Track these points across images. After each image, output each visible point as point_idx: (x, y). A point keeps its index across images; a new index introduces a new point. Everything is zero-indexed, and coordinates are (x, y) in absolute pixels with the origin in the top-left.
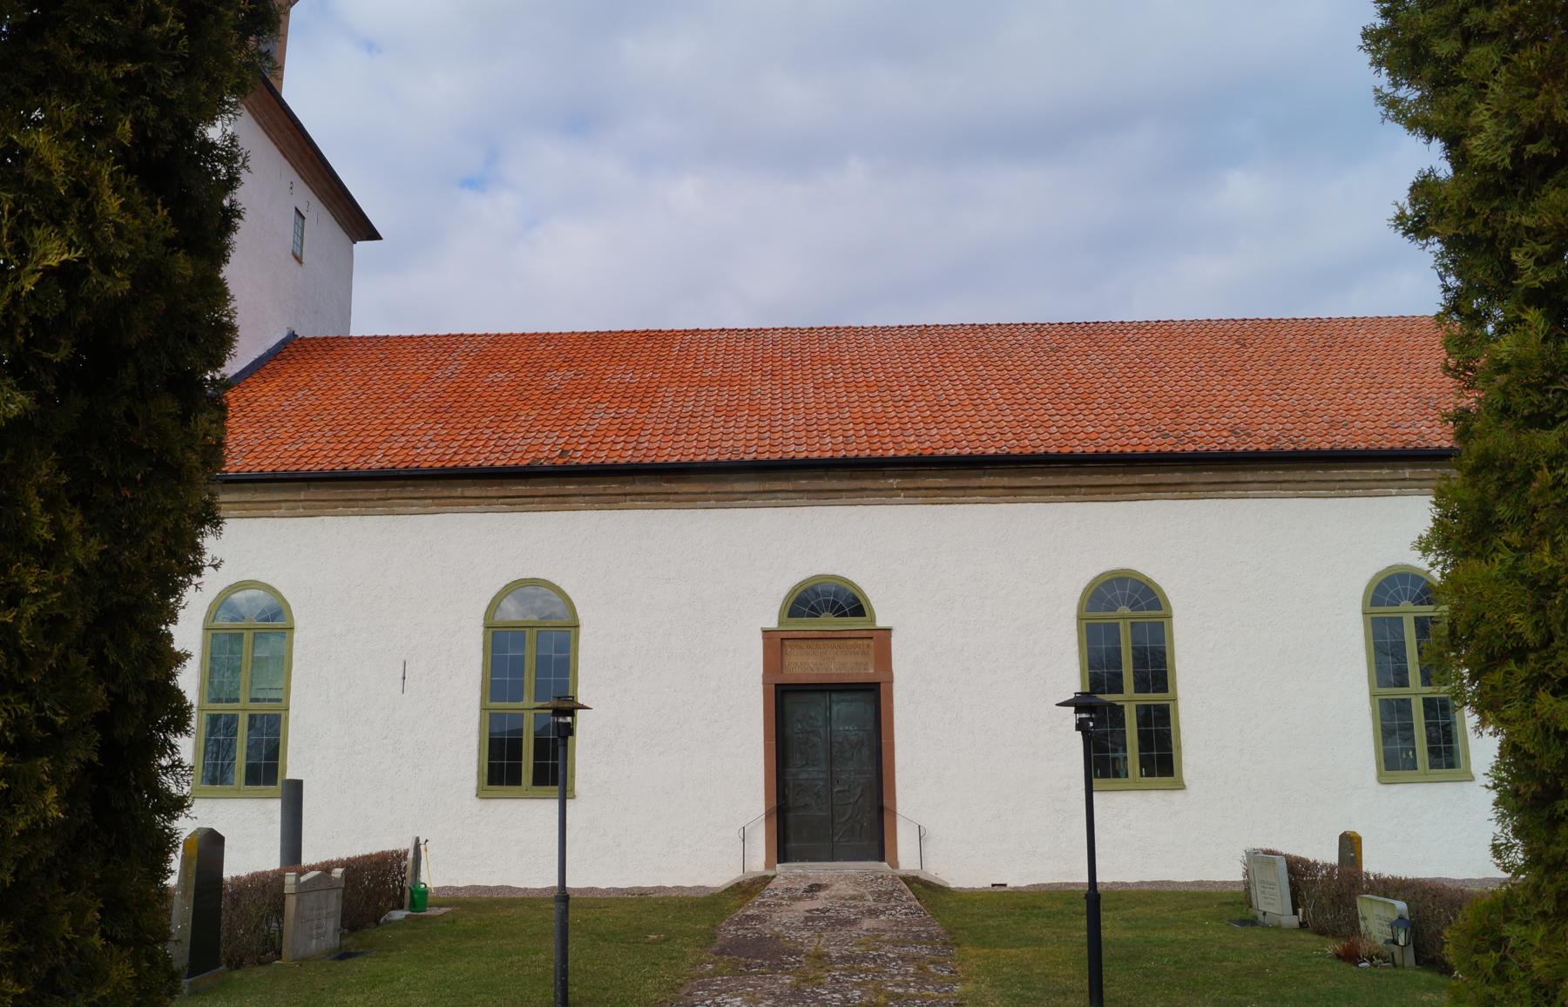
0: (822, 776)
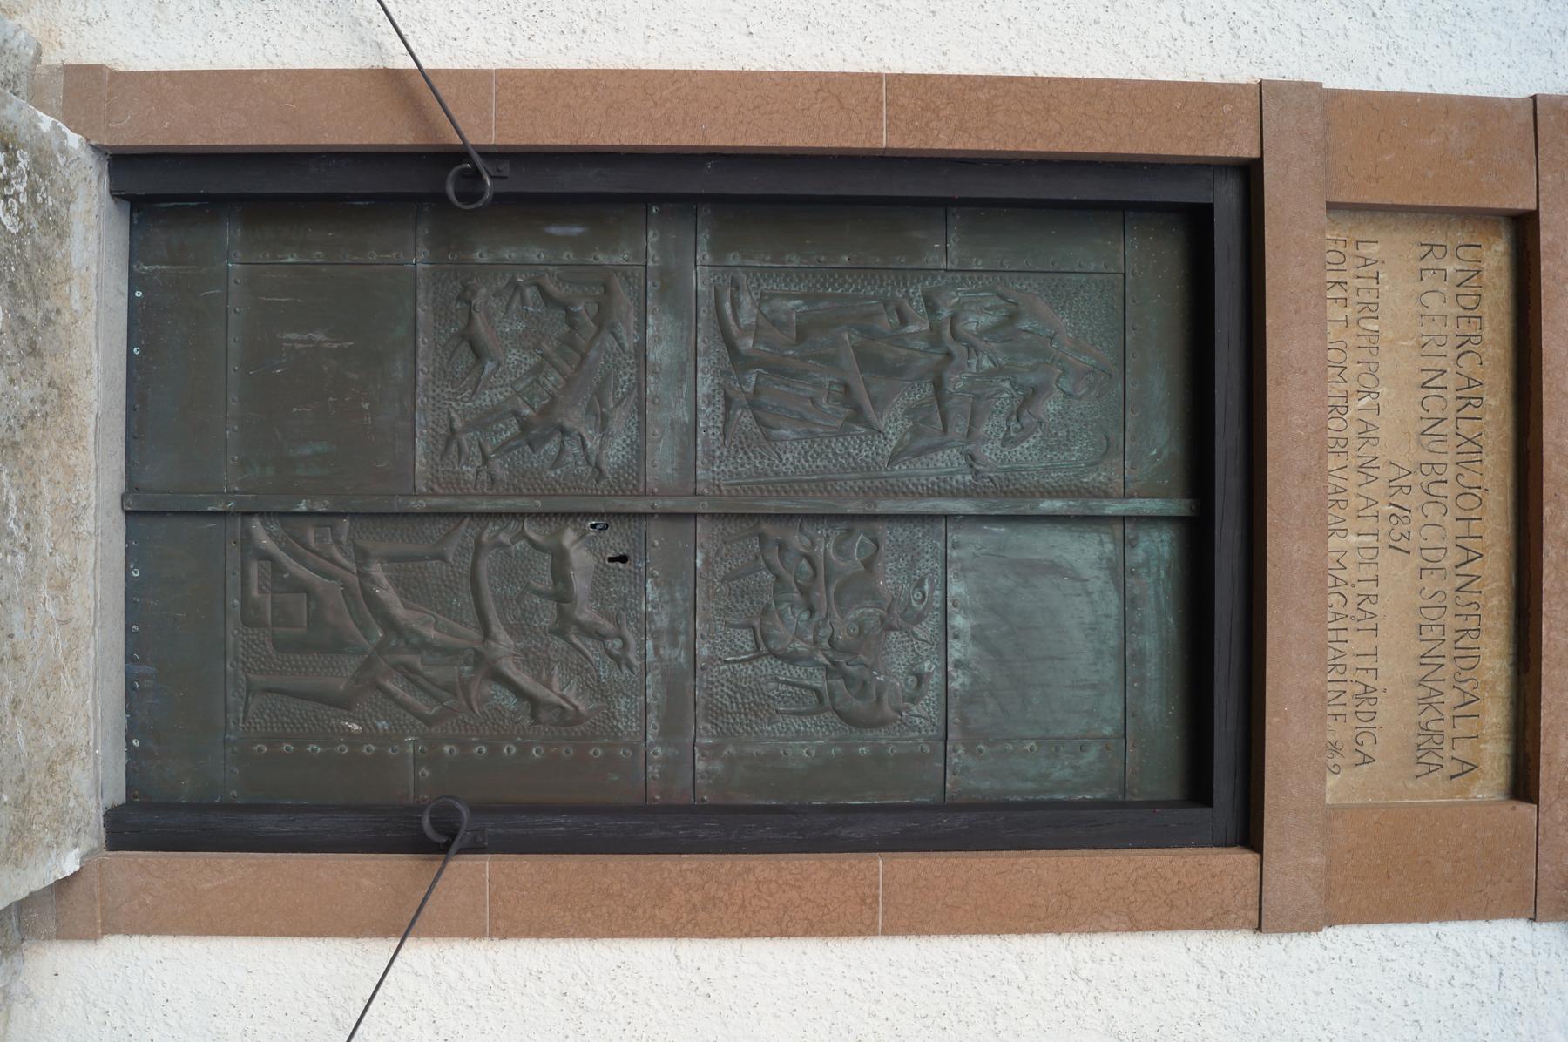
0: (662, 460)
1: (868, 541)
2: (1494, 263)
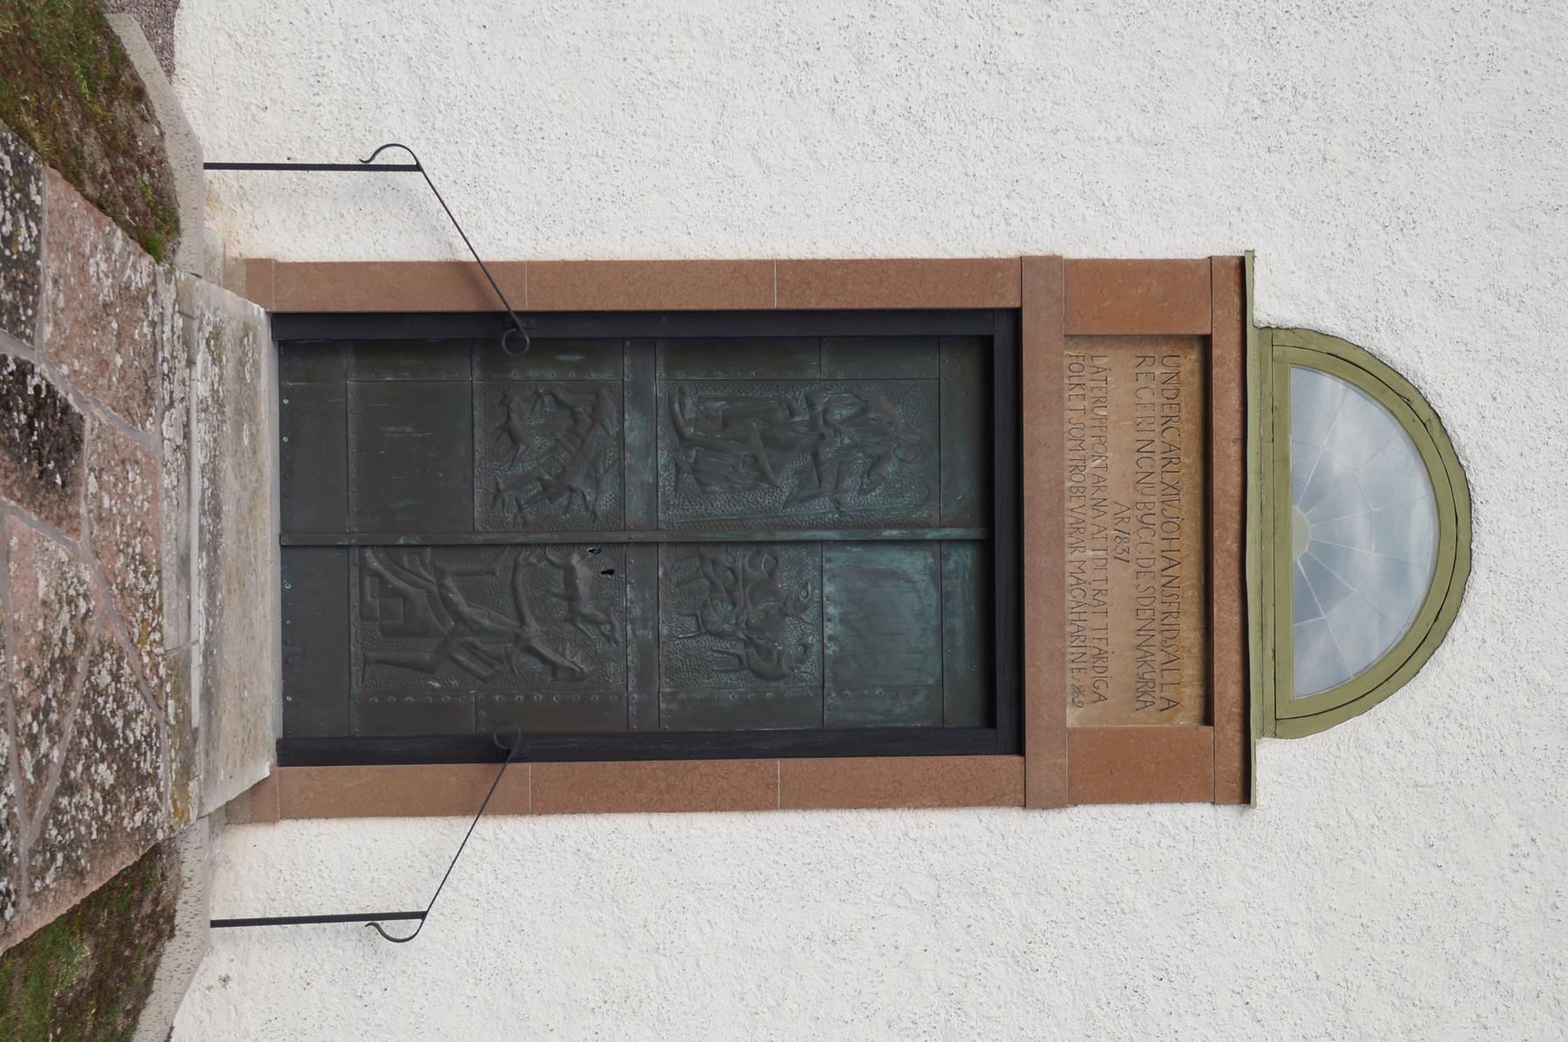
0: (636, 505)
1: (770, 558)
2: (1188, 367)
